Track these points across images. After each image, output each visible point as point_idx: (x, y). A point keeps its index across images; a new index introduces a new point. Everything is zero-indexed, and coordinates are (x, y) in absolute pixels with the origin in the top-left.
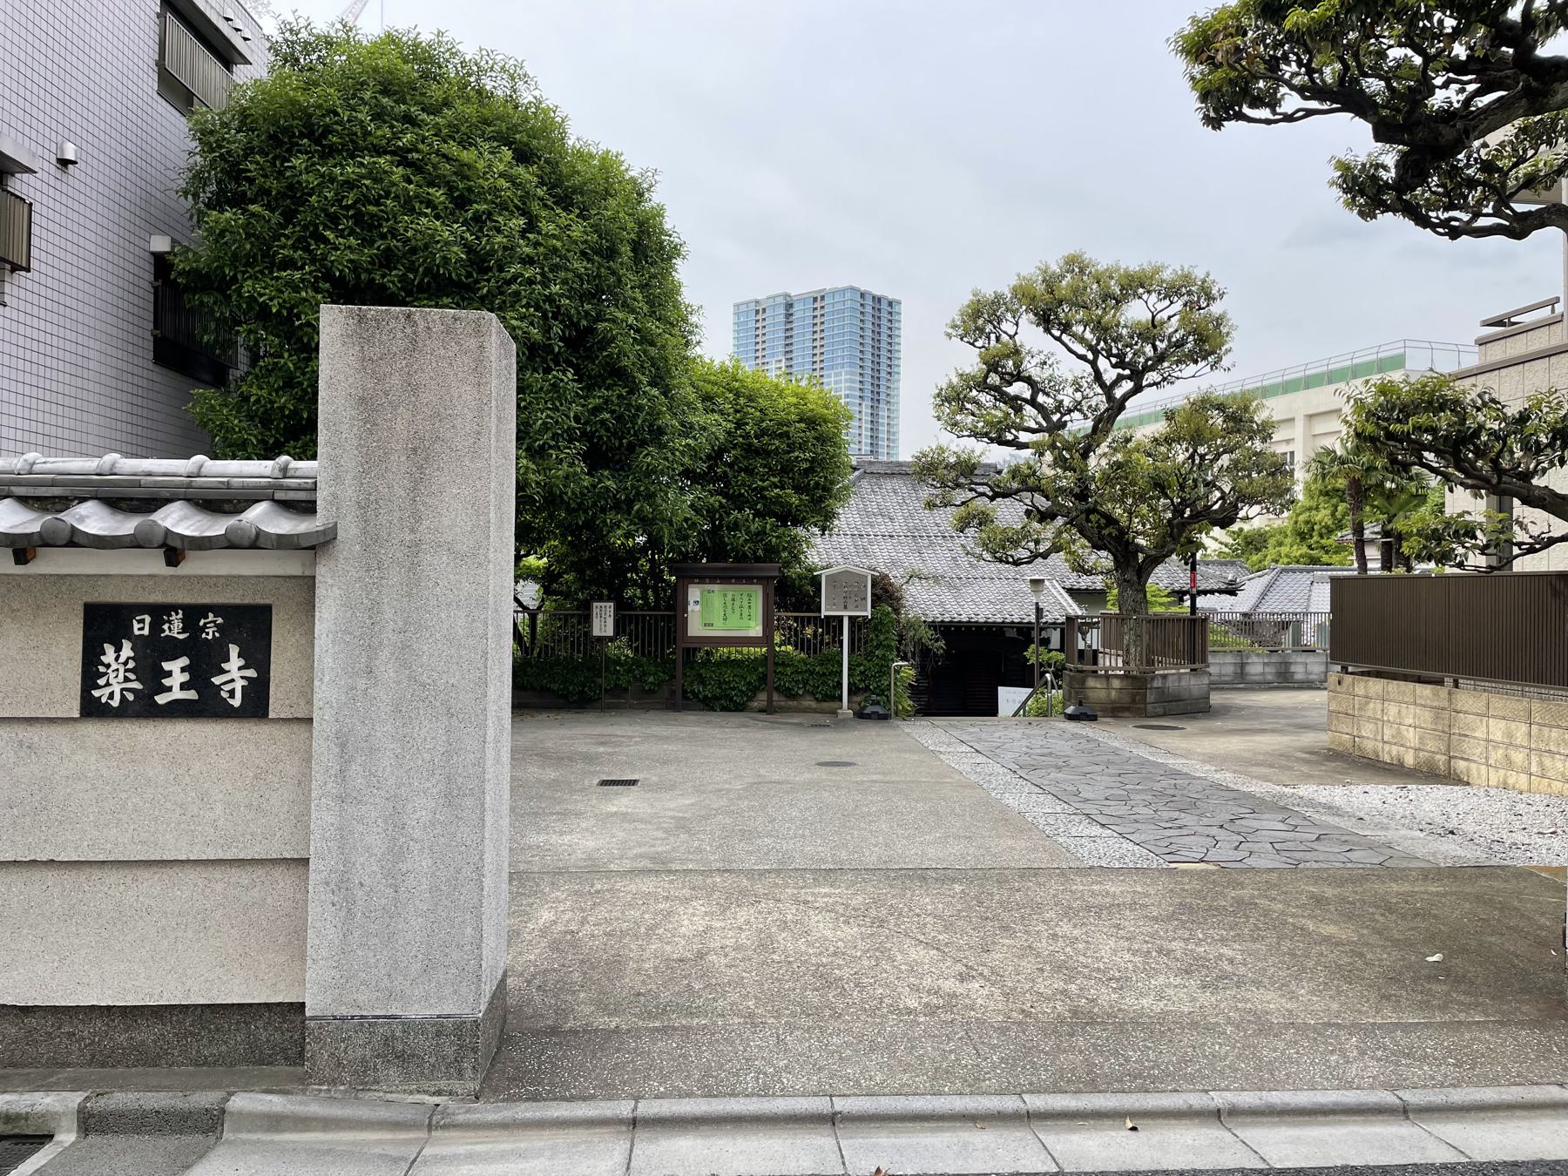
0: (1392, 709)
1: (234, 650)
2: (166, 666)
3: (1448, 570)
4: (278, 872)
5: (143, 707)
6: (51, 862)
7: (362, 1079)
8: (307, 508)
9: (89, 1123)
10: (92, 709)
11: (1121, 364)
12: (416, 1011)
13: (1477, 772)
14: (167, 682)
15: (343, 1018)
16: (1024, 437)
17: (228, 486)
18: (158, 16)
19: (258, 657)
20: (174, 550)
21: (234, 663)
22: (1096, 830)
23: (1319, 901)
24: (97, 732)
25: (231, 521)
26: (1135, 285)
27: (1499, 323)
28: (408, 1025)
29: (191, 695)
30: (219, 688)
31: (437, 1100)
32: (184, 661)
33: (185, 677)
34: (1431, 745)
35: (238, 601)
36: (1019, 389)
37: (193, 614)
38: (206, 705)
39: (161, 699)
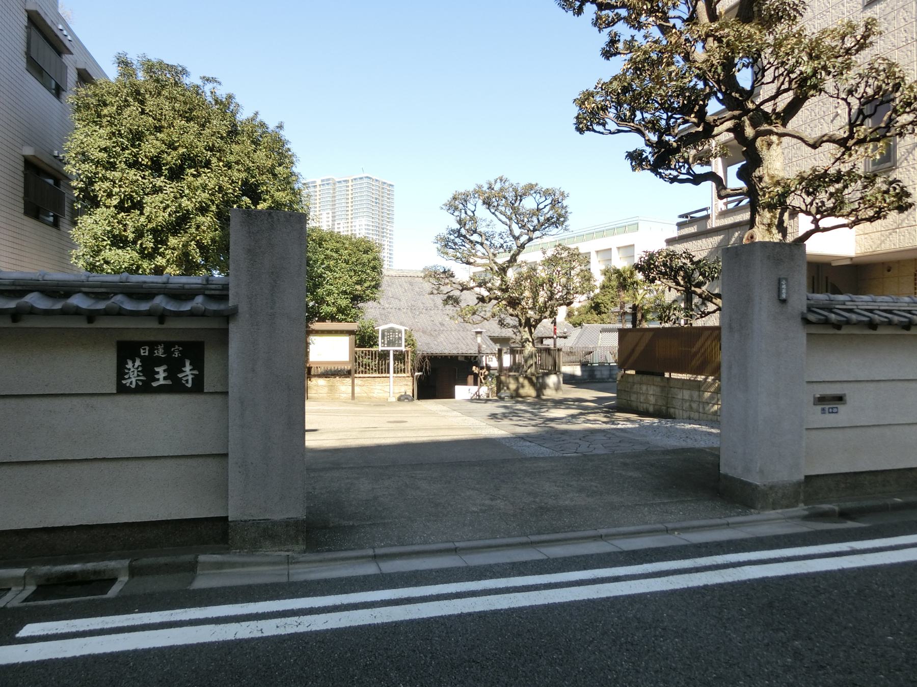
0: (644, 388)
1: (188, 363)
2: (157, 369)
3: (667, 325)
4: (209, 460)
5: (145, 388)
6: (104, 459)
7: (254, 546)
8: (224, 298)
9: (133, 572)
10: (123, 389)
11: (523, 227)
12: (277, 517)
13: (679, 413)
14: (157, 376)
15: (245, 521)
16: (479, 261)
17: (183, 288)
18: (26, 27)
19: (198, 365)
20: (162, 316)
21: (188, 368)
22: (528, 444)
23: (625, 464)
24: (124, 400)
25: (109, 303)
26: (530, 189)
27: (686, 216)
28: (274, 523)
29: (168, 382)
30: (181, 379)
31: (287, 553)
32: (164, 367)
33: (165, 374)
34: (660, 403)
35: (193, 340)
36: (475, 238)
37: (168, 346)
38: (175, 387)
39: (155, 384)
